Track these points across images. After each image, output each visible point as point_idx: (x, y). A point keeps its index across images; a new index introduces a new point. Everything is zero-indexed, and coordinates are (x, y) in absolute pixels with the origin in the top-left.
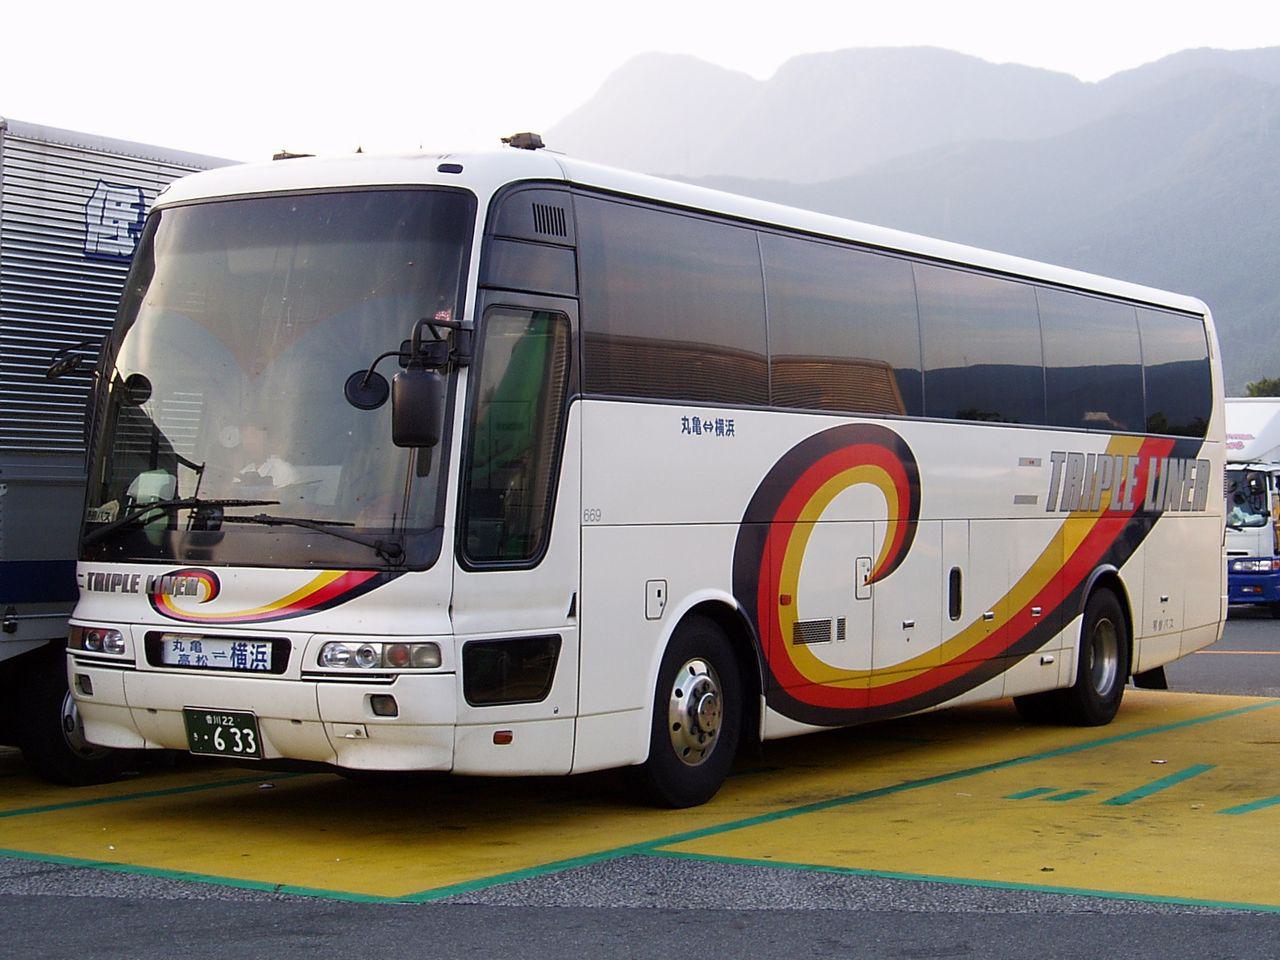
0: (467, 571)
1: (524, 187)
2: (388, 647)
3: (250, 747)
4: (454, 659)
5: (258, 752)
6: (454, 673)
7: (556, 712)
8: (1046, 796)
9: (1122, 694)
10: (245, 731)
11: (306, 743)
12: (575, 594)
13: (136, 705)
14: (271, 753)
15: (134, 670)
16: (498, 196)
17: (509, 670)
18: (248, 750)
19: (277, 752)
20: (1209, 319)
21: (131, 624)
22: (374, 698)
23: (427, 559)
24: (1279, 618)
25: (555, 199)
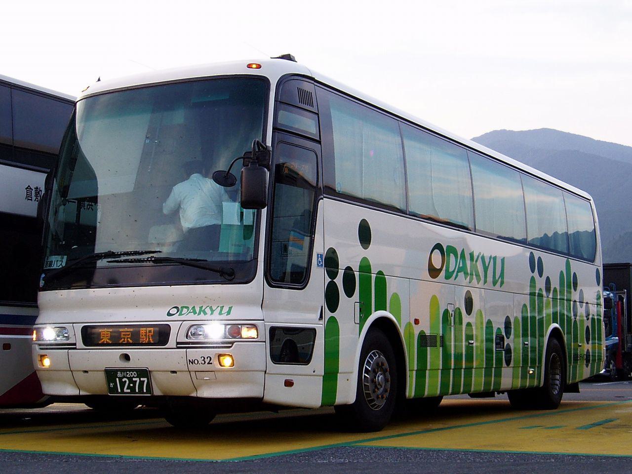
0: (271, 287)
1: (293, 78)
2: (229, 327)
4: (172, 342)
6: (265, 342)
7: (314, 372)
10: (142, 379)
11: (179, 385)
12: (322, 307)
13: (75, 369)
14: (157, 392)
15: (75, 349)
17: (289, 346)
19: (159, 391)
20: (592, 202)
21: (73, 323)
23: (252, 276)
24: (630, 379)
25: (307, 86)
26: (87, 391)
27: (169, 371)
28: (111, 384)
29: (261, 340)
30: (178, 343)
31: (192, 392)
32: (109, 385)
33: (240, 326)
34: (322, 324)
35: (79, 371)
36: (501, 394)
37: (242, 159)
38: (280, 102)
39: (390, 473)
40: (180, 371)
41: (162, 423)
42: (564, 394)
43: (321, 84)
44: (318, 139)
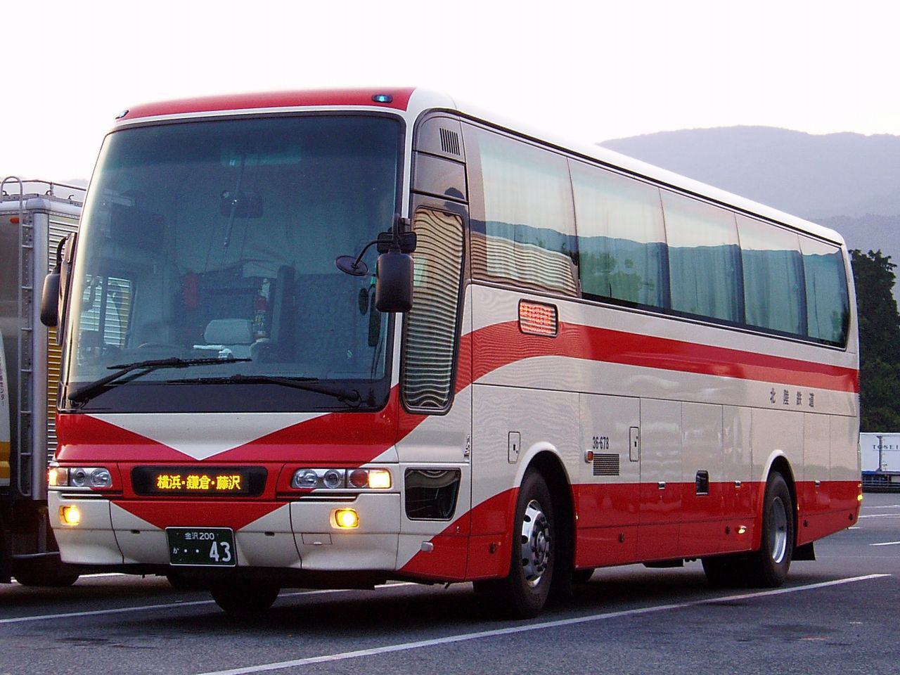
3: (226, 556)
5: (232, 561)
6: (400, 493)
8: (828, 638)
9: (78, 577)
10: (222, 544)
13: (119, 528)
14: (242, 561)
16: (416, 125)
18: (224, 559)
22: (615, 471)
25: (452, 125)
26: (136, 560)
27: (263, 532)
28: (175, 550)
29: (394, 491)
30: (278, 494)
31: (294, 561)
32: (171, 550)
33: (367, 471)
34: (468, 463)
35: (127, 530)
36: (691, 561)
37: (376, 244)
38: (419, 152)
39: (38, 673)
40: (278, 532)
41: (208, 602)
42: (792, 562)
43: (486, 125)
44: (466, 201)
